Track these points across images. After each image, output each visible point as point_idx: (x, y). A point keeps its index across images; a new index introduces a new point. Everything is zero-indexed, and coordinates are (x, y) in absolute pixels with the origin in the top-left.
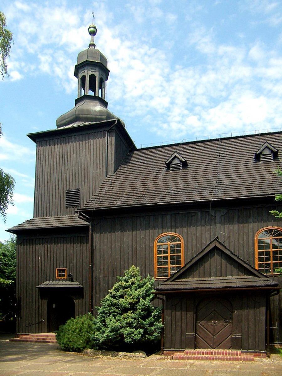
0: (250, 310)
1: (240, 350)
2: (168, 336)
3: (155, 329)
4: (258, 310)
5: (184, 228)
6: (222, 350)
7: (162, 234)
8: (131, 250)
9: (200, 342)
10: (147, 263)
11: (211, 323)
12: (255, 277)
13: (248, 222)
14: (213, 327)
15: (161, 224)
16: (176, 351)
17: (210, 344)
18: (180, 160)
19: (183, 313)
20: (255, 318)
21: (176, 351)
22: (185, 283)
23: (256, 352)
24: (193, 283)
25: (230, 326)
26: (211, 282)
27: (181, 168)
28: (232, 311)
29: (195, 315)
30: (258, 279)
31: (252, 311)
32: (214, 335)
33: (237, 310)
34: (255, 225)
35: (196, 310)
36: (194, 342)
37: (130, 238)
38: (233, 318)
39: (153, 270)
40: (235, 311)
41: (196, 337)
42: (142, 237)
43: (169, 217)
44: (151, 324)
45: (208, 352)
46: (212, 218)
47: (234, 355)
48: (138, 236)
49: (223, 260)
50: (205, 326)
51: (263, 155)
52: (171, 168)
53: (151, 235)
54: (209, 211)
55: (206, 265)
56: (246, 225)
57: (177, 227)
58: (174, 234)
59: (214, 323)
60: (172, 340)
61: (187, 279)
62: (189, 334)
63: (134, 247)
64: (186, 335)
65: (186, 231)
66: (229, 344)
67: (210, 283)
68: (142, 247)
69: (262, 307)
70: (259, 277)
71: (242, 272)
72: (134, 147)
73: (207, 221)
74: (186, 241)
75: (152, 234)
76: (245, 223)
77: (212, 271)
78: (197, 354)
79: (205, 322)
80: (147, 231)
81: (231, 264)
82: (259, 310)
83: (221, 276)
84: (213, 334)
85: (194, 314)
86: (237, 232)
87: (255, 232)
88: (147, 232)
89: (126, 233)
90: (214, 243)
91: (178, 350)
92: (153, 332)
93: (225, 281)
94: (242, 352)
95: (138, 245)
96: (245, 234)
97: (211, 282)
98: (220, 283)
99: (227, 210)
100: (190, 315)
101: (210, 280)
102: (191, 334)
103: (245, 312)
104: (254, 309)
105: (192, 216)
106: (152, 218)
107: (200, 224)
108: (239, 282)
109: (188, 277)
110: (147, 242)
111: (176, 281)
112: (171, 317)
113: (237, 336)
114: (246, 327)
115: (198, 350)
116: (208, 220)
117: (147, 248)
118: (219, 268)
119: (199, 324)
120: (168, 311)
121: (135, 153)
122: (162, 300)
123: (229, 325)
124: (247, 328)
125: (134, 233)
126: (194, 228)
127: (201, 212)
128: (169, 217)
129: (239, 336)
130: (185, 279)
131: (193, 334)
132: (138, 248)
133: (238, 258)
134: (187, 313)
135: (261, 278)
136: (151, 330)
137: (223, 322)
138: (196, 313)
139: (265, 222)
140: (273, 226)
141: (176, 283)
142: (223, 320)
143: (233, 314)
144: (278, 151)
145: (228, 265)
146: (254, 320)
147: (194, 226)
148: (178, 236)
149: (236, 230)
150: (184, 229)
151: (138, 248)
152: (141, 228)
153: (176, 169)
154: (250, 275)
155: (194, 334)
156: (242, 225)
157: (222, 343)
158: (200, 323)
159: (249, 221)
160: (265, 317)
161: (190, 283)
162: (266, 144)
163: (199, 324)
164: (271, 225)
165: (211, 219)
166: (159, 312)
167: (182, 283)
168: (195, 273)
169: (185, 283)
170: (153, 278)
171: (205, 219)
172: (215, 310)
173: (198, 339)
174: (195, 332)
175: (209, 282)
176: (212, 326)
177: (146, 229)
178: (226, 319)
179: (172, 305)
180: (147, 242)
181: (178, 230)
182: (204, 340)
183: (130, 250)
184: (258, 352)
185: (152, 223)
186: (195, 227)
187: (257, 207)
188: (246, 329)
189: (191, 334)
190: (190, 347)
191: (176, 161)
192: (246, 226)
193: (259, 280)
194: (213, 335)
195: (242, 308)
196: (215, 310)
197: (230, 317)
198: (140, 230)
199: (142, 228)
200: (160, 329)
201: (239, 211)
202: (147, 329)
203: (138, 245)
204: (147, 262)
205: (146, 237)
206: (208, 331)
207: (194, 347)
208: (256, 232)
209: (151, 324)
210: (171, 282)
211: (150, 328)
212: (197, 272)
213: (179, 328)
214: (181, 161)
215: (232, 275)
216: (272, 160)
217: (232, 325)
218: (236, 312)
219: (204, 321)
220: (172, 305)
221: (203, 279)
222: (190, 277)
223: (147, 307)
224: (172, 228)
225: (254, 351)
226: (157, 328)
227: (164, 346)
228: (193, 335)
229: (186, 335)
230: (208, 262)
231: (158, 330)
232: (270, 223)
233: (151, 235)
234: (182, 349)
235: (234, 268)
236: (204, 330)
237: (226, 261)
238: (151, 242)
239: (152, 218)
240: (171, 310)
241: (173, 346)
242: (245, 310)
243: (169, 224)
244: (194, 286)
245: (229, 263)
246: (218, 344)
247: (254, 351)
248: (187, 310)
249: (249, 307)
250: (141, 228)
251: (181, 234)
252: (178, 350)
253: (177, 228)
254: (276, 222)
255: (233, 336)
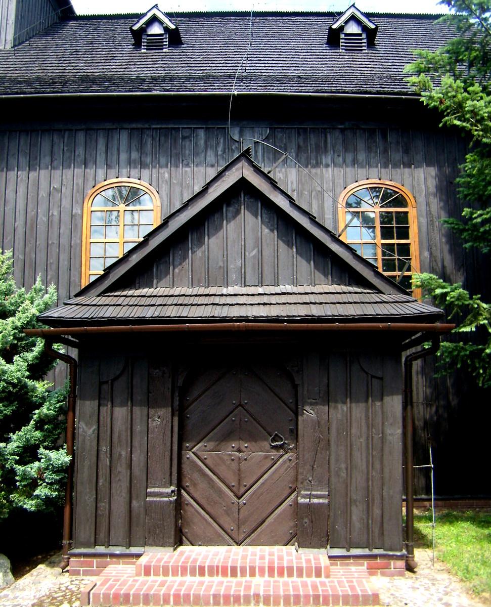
0: (353, 405)
1: (323, 550)
2: (84, 496)
3: (40, 471)
4: (378, 404)
5: (162, 167)
6: (267, 549)
7: (106, 183)
8: (22, 223)
9: (196, 520)
10: (64, 263)
11: (229, 451)
12: (365, 291)
13: (321, 163)
14: (234, 465)
15: (103, 156)
16: (113, 556)
17: (226, 526)
18: (165, 25)
19: (137, 410)
20: (372, 429)
21: (113, 556)
22: (143, 301)
23: (375, 557)
24: (170, 301)
25: (290, 460)
26: (229, 300)
27: (166, 45)
28: (297, 408)
29: (176, 419)
30: (376, 297)
31: (358, 410)
32: (243, 490)
33: (311, 404)
34: (339, 172)
35: (181, 401)
36: (173, 520)
37: (22, 190)
38: (300, 432)
39: (77, 280)
40: (307, 408)
41: (179, 504)
42: (54, 187)
43: (124, 136)
44: (29, 453)
45: (218, 567)
46: (233, 147)
47: (309, 576)
48: (44, 184)
49: (266, 231)
50: (207, 461)
51: (346, 35)
52: (144, 42)
53: (78, 184)
54: (225, 128)
55: (213, 243)
56: (318, 171)
57: (143, 165)
58: (134, 182)
59: (239, 451)
60: (99, 512)
61: (152, 290)
62: (157, 490)
63: (31, 214)
64: (147, 494)
65: (167, 175)
66: (287, 527)
67: (224, 305)
68: (53, 214)
69: (392, 394)
70: (380, 292)
71: (326, 275)
72: (71, 10)
73: (220, 153)
74: (165, 203)
75: (81, 181)
76: (314, 167)
77: (231, 266)
78: (182, 575)
79: (211, 445)
80: (68, 173)
81: (289, 244)
82: (382, 406)
83: (261, 283)
84: (234, 489)
85: (173, 415)
86: (294, 187)
87: (338, 190)
88: (66, 176)
89: (12, 175)
90: (237, 170)
91: (118, 550)
92: (34, 484)
93: (273, 299)
94: (330, 557)
95: (42, 210)
96: (313, 194)
97: (229, 300)
98: (259, 304)
99: (270, 129)
100: (160, 420)
101: (226, 295)
102: (162, 493)
103: (339, 411)
104: (367, 401)
105: (184, 138)
106: (81, 137)
107: (203, 159)
108: (321, 303)
109: (155, 281)
110: (66, 203)
111: (116, 294)
112: (95, 427)
113: (315, 501)
114: (343, 466)
115: (187, 551)
116: (224, 152)
117: (66, 218)
118: (254, 257)
119: (190, 455)
120: (88, 403)
121: (72, 23)
122: (71, 363)
123: (286, 457)
124: (347, 469)
125: (33, 175)
126: (188, 169)
127: (207, 129)
128: (124, 136)
129: (321, 501)
130: (145, 291)
131: (169, 490)
132: (42, 218)
133: (312, 219)
134: (152, 412)
135: (384, 294)
136: (25, 476)
137: (268, 447)
138: (181, 412)
139: (362, 167)
140: (380, 179)
141: (113, 301)
142: (266, 440)
143: (300, 418)
144: (377, 27)
145: (282, 246)
146: (368, 439)
147: (188, 165)
148: (147, 191)
149: (292, 183)
150: (162, 171)
151: (42, 218)
152: (52, 162)
153: (155, 44)
154: (349, 285)
155: (173, 491)
156: (306, 171)
157: (264, 521)
158: (193, 450)
159: (324, 162)
160: (400, 431)
161: (160, 301)
162: (352, 10)
163: (190, 455)
164: (376, 176)
165: (232, 149)
166: (58, 405)
167: (133, 301)
168: (177, 270)
169: (143, 301)
170: (52, 289)
171: (216, 148)
172: (240, 405)
173: (186, 508)
174: (175, 481)
175: (223, 300)
176: (233, 463)
177: (66, 165)
178: (276, 435)
179: (101, 383)
180: (66, 203)
181: (146, 173)
182: (208, 513)
183: (20, 223)
184: (382, 556)
185: (80, 151)
186: (190, 167)
187: (342, 127)
188: (343, 475)
189: (162, 493)
190: (159, 542)
191: (156, 29)
192: (316, 174)
193: (379, 300)
194: (236, 495)
195: (327, 398)
196: (242, 403)
197: (291, 431)
198: (48, 168)
199: (55, 163)
200: (58, 470)
201: (299, 133)
202: (13, 472)
203: (42, 210)
204: (64, 257)
205: (64, 189)
206: (219, 478)
207: (172, 540)
208: (341, 193)
209: (29, 453)
210: (98, 296)
211: (19, 469)
212: (187, 264)
213: (121, 468)
214: (166, 29)
215: (295, 283)
216: (365, 48)
217: (297, 458)
218: (310, 413)
219: (208, 441)
220: (101, 383)
221: (202, 291)
222: (162, 283)
223: (14, 386)
224: (132, 165)
225: (366, 552)
226: (47, 469)
227: (71, 538)
228: (168, 495)
229: (147, 494)
230: (220, 234)
231: (49, 476)
232: (374, 171)
233: (78, 184)
234: (134, 550)
235: (299, 258)
236: (204, 475)
237: (276, 232)
238: (77, 202)
239: (81, 137)
240: (97, 402)
241: (102, 535)
242: (339, 406)
243: (123, 156)
244: (172, 312)
245: (284, 242)
246: (254, 525)
247: (366, 552)
248: (151, 402)
249: (349, 395)
250: (52, 162)
251: (154, 184)
252: (118, 550)
253: (144, 168)
254: (387, 170)
255: (301, 500)
